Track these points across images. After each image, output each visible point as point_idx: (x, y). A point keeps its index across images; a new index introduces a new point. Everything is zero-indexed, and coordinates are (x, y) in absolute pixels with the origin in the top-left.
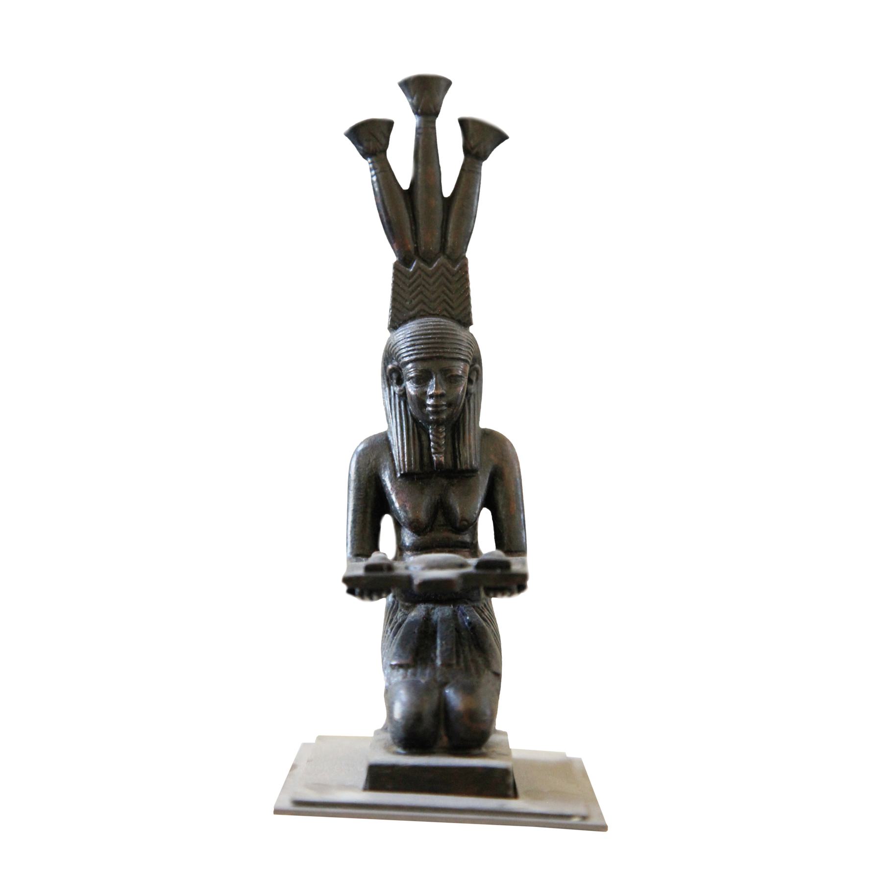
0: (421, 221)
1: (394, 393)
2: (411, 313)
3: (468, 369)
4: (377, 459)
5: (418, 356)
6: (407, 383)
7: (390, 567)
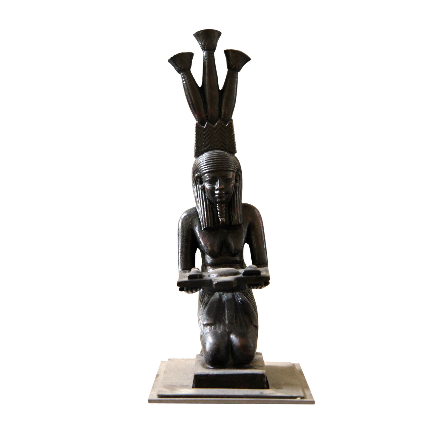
1: (199, 188)
4: (192, 221)
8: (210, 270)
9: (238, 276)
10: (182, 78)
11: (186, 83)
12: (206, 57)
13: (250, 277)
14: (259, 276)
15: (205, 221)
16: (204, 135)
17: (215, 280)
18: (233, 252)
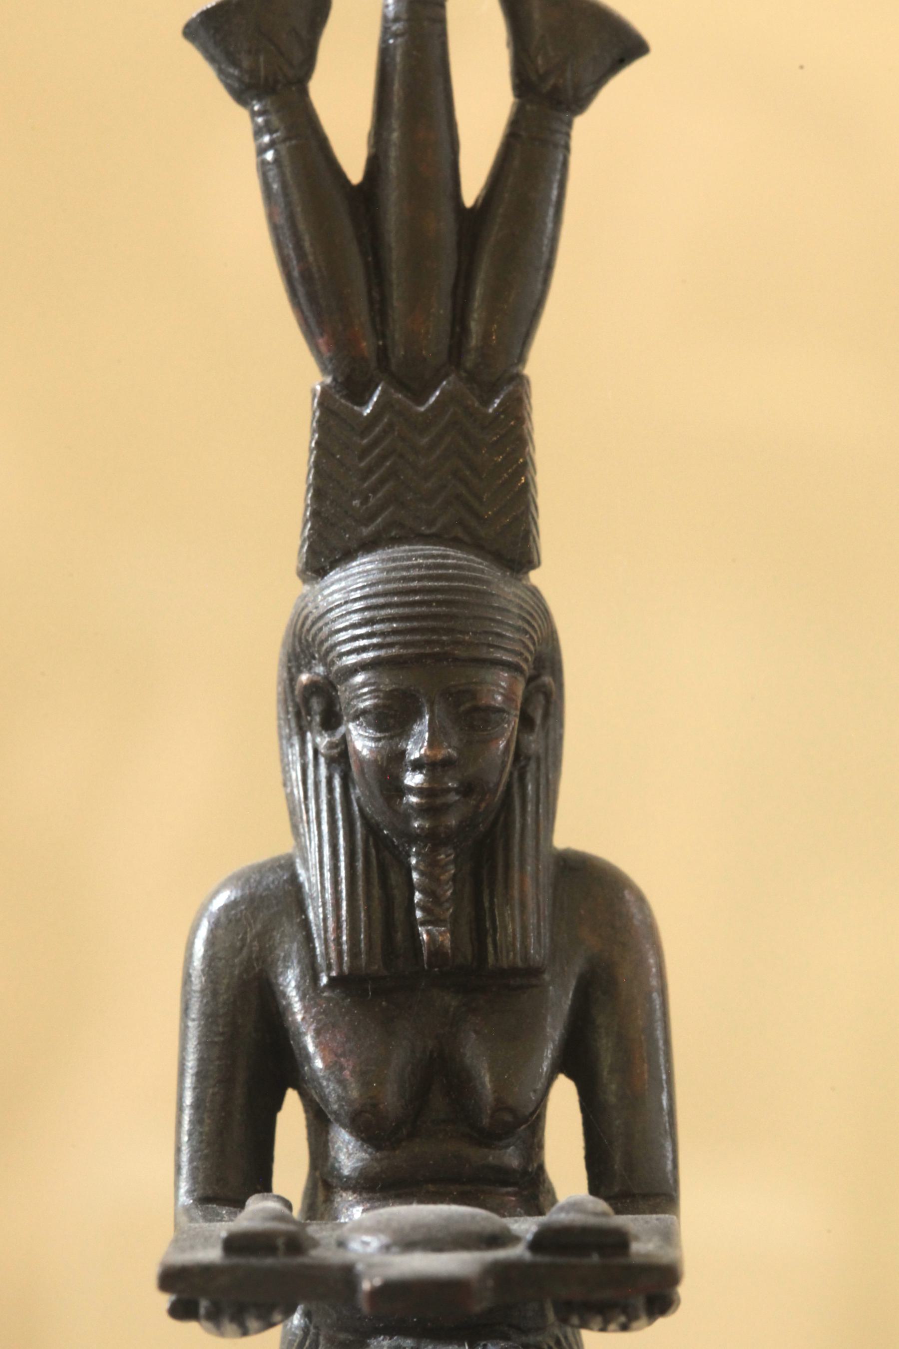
0: (395, 276)
1: (316, 752)
2: (366, 531)
3: (520, 689)
4: (264, 935)
5: (382, 653)
6: (351, 726)
7: (296, 1244)
8: (354, 1212)
9: (501, 1254)
10: (258, 132)
11: (277, 160)
12: (396, 19)
13: (574, 1260)
14: (621, 1261)
15: (338, 939)
16: (365, 452)
17: (370, 1266)
18: (486, 1121)
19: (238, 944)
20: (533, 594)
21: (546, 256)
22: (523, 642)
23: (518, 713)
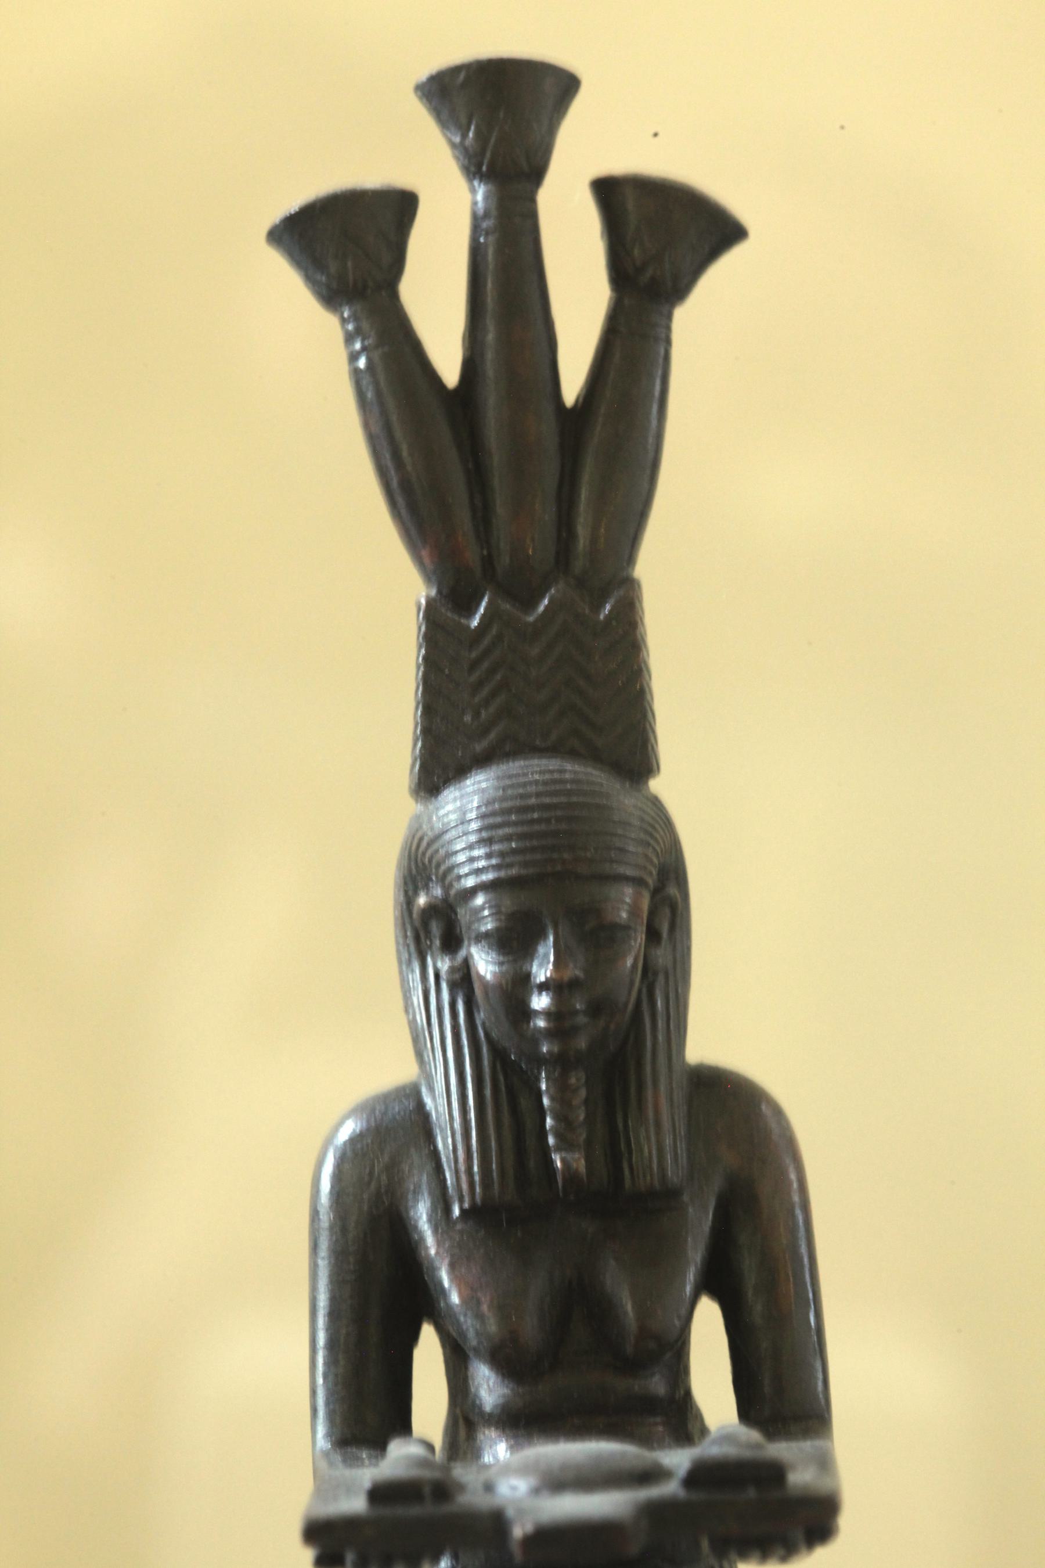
1: (437, 976)
2: (479, 747)
3: (645, 904)
4: (393, 1167)
8: (498, 1450)
10: (349, 339)
12: (486, 215)
16: (474, 665)
17: (521, 1512)
19: (366, 1179)
20: (654, 804)
21: (651, 455)
22: (646, 856)
23: (644, 929)
